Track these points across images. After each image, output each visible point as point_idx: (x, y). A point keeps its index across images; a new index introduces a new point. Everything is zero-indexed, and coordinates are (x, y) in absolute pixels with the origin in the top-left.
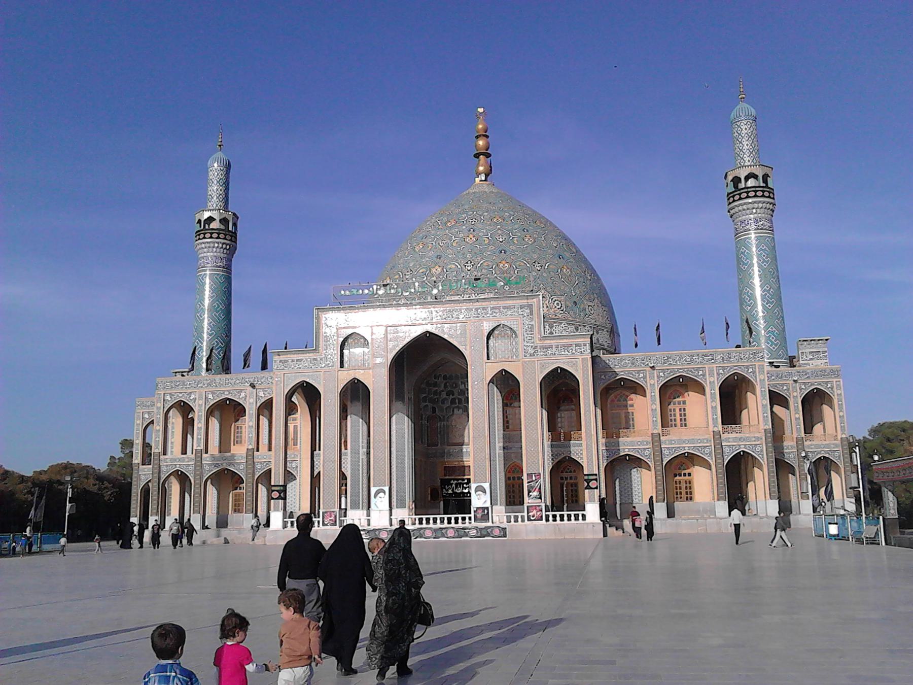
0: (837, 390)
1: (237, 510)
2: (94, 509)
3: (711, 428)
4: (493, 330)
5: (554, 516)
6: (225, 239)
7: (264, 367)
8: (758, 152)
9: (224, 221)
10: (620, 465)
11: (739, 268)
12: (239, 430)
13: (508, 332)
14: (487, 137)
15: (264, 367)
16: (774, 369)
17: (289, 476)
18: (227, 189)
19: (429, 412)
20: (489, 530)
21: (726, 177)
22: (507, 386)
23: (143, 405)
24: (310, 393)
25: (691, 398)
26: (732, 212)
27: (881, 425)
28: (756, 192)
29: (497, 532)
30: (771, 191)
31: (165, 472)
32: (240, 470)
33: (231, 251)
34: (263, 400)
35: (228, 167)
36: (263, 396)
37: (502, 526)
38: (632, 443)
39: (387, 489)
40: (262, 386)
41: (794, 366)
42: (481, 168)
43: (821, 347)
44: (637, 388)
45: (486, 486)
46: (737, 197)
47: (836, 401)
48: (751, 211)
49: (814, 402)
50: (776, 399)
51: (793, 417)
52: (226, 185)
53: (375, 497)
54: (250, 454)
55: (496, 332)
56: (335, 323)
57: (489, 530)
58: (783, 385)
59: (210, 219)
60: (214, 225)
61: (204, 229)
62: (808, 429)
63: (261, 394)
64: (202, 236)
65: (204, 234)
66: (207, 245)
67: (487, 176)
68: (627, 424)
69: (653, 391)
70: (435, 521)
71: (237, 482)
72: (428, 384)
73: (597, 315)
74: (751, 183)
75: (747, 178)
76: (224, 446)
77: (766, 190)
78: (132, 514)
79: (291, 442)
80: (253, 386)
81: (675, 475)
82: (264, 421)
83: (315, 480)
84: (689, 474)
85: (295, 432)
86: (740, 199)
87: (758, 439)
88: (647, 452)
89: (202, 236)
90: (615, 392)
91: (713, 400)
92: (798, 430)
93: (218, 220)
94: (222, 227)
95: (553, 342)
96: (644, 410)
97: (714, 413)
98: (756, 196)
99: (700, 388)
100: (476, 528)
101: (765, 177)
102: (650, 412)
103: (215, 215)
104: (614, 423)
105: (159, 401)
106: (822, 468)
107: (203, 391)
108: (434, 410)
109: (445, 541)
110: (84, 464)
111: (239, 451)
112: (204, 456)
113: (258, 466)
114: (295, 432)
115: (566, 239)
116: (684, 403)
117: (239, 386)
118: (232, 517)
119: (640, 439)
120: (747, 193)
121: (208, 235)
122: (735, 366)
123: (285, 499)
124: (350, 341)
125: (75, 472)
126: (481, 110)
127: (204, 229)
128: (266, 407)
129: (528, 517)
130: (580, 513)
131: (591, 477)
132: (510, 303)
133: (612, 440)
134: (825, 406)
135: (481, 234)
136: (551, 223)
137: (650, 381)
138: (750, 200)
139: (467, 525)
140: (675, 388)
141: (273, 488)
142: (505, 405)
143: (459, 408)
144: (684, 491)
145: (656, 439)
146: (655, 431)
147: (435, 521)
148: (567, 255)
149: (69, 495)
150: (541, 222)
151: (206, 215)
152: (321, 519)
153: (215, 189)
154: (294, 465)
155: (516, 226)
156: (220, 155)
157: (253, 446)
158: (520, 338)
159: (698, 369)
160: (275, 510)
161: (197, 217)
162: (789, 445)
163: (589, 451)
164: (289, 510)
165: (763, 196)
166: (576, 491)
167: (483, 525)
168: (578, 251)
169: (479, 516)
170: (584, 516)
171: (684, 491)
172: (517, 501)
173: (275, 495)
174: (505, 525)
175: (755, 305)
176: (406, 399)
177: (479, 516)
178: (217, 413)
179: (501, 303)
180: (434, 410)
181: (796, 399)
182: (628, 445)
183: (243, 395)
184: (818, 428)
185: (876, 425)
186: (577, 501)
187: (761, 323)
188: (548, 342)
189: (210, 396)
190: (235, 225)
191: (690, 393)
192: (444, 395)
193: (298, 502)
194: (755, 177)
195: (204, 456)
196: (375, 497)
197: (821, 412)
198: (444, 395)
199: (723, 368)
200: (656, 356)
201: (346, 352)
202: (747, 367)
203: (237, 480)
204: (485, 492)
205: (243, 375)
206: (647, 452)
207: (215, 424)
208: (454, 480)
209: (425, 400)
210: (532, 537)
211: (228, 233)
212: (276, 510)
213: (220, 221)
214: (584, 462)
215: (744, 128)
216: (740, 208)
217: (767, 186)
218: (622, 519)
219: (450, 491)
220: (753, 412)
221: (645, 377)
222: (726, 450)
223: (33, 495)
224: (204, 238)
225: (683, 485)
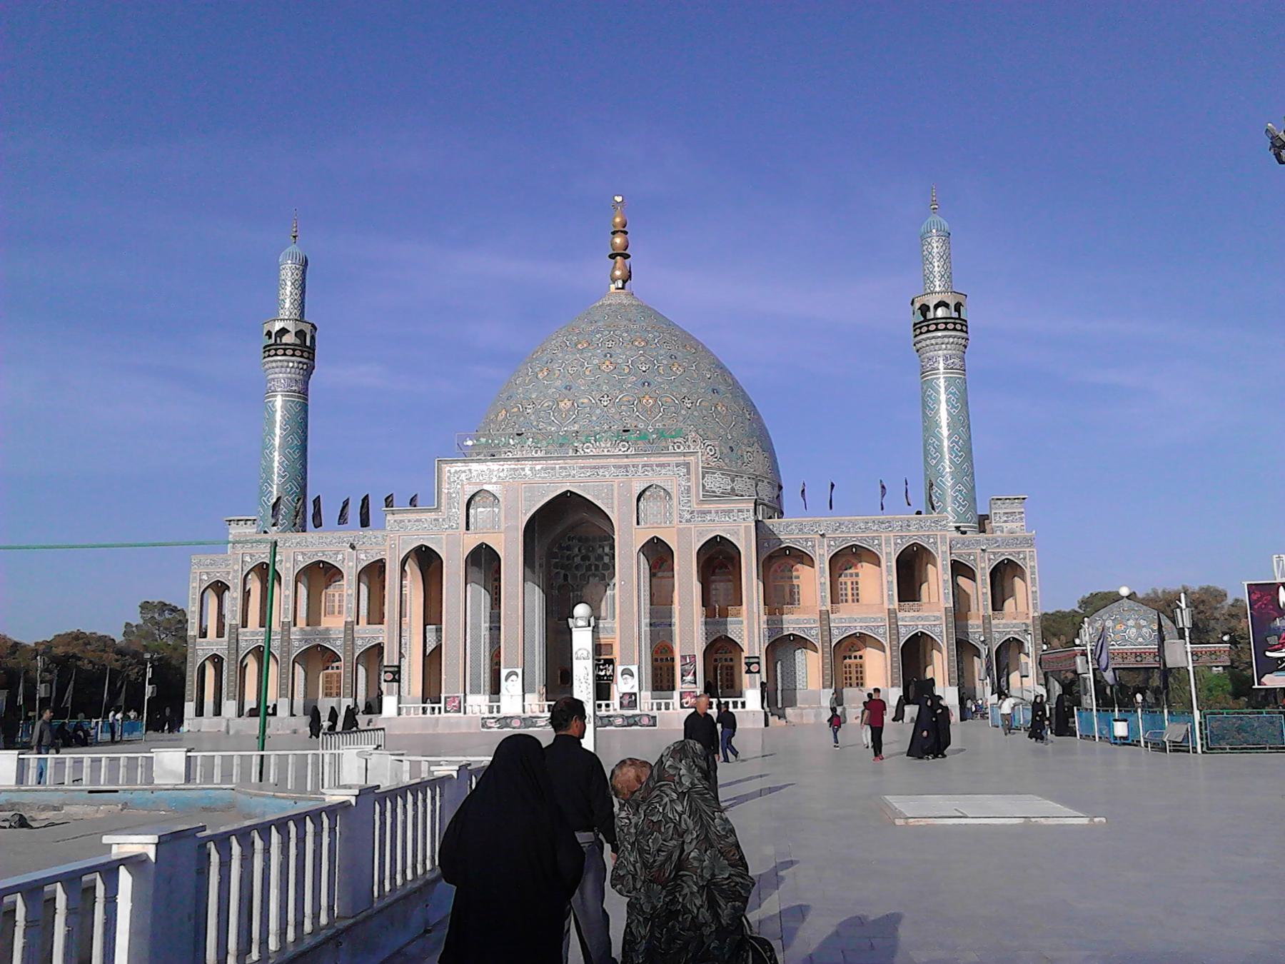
0: (1030, 561)
2: (110, 688)
3: (886, 606)
4: (644, 491)
5: (433, 709)
7: (365, 523)
8: (948, 276)
9: (300, 334)
10: (783, 646)
11: (924, 413)
13: (662, 493)
14: (626, 233)
15: (365, 523)
16: (959, 535)
18: (303, 292)
19: (561, 581)
21: (912, 303)
22: (658, 555)
23: (199, 564)
24: (427, 560)
25: (865, 569)
26: (919, 346)
27: (1094, 596)
28: (946, 324)
29: (645, 721)
30: (964, 323)
31: (245, 646)
32: (337, 647)
33: (309, 371)
37: (651, 714)
38: (797, 622)
39: (519, 671)
40: (363, 547)
41: (984, 532)
42: (618, 273)
43: (1017, 508)
44: (804, 558)
45: (634, 669)
46: (925, 329)
47: (1028, 572)
48: (941, 349)
49: (1004, 574)
50: (960, 569)
51: (979, 591)
52: (302, 287)
53: (506, 680)
55: (647, 493)
56: (462, 476)
58: (969, 555)
59: (283, 331)
60: (288, 339)
61: (274, 345)
62: (997, 605)
63: (363, 556)
64: (272, 352)
67: (624, 282)
68: (791, 598)
69: (822, 564)
72: (561, 548)
73: (758, 463)
74: (940, 312)
75: (936, 307)
77: (959, 324)
78: (187, 697)
80: (353, 547)
81: (845, 658)
83: (432, 660)
86: (928, 331)
87: (937, 618)
88: (814, 632)
89: (272, 352)
90: (780, 560)
91: (889, 573)
92: (985, 607)
94: (298, 342)
95: (713, 507)
96: (811, 583)
97: (890, 589)
98: (946, 329)
99: (877, 561)
101: (958, 307)
102: (818, 586)
103: (290, 326)
104: (778, 598)
105: (236, 562)
106: (1011, 647)
107: (296, 551)
108: (566, 577)
110: (100, 633)
111: (333, 624)
112: (293, 629)
113: (359, 642)
115: (722, 368)
116: (857, 575)
117: (343, 548)
119: (806, 617)
120: (937, 324)
122: (915, 535)
123: (399, 681)
124: (477, 499)
125: (89, 644)
126: (619, 199)
127: (274, 345)
132: (663, 460)
133: (774, 617)
134: (1016, 579)
135: (620, 361)
136: (703, 347)
138: (939, 334)
139: (612, 712)
140: (847, 558)
142: (652, 575)
143: (595, 576)
144: (854, 676)
145: (825, 617)
146: (824, 608)
148: (722, 388)
149: (149, 675)
150: (692, 347)
151: (278, 326)
152: (442, 705)
153: (288, 292)
155: (662, 352)
156: (293, 248)
157: (352, 618)
158: (675, 500)
159: (873, 538)
161: (267, 328)
162: (975, 624)
163: (749, 629)
165: (954, 329)
166: (732, 674)
167: (630, 712)
168: (735, 383)
169: (626, 702)
170: (743, 704)
171: (854, 676)
172: (665, 684)
174: (655, 712)
175: (942, 459)
176: (537, 566)
177: (626, 702)
178: (304, 579)
179: (654, 460)
180: (566, 577)
181: (983, 570)
182: (792, 623)
183: (340, 557)
184: (1009, 603)
185: (1087, 595)
186: (732, 687)
187: (949, 481)
188: (706, 507)
189: (300, 558)
190: (313, 338)
192: (578, 560)
194: (946, 305)
195: (293, 629)
196: (506, 680)
197: (1013, 584)
198: (578, 560)
199: (902, 538)
200: (827, 522)
201: (472, 511)
202: (928, 537)
204: (632, 675)
205: (337, 534)
206: (814, 632)
207: (303, 591)
209: (556, 566)
214: (745, 645)
215: (936, 246)
216: (928, 342)
217: (959, 318)
218: (783, 708)
220: (934, 587)
221: (813, 546)
222: (902, 630)
223: (51, 672)
225: (853, 669)
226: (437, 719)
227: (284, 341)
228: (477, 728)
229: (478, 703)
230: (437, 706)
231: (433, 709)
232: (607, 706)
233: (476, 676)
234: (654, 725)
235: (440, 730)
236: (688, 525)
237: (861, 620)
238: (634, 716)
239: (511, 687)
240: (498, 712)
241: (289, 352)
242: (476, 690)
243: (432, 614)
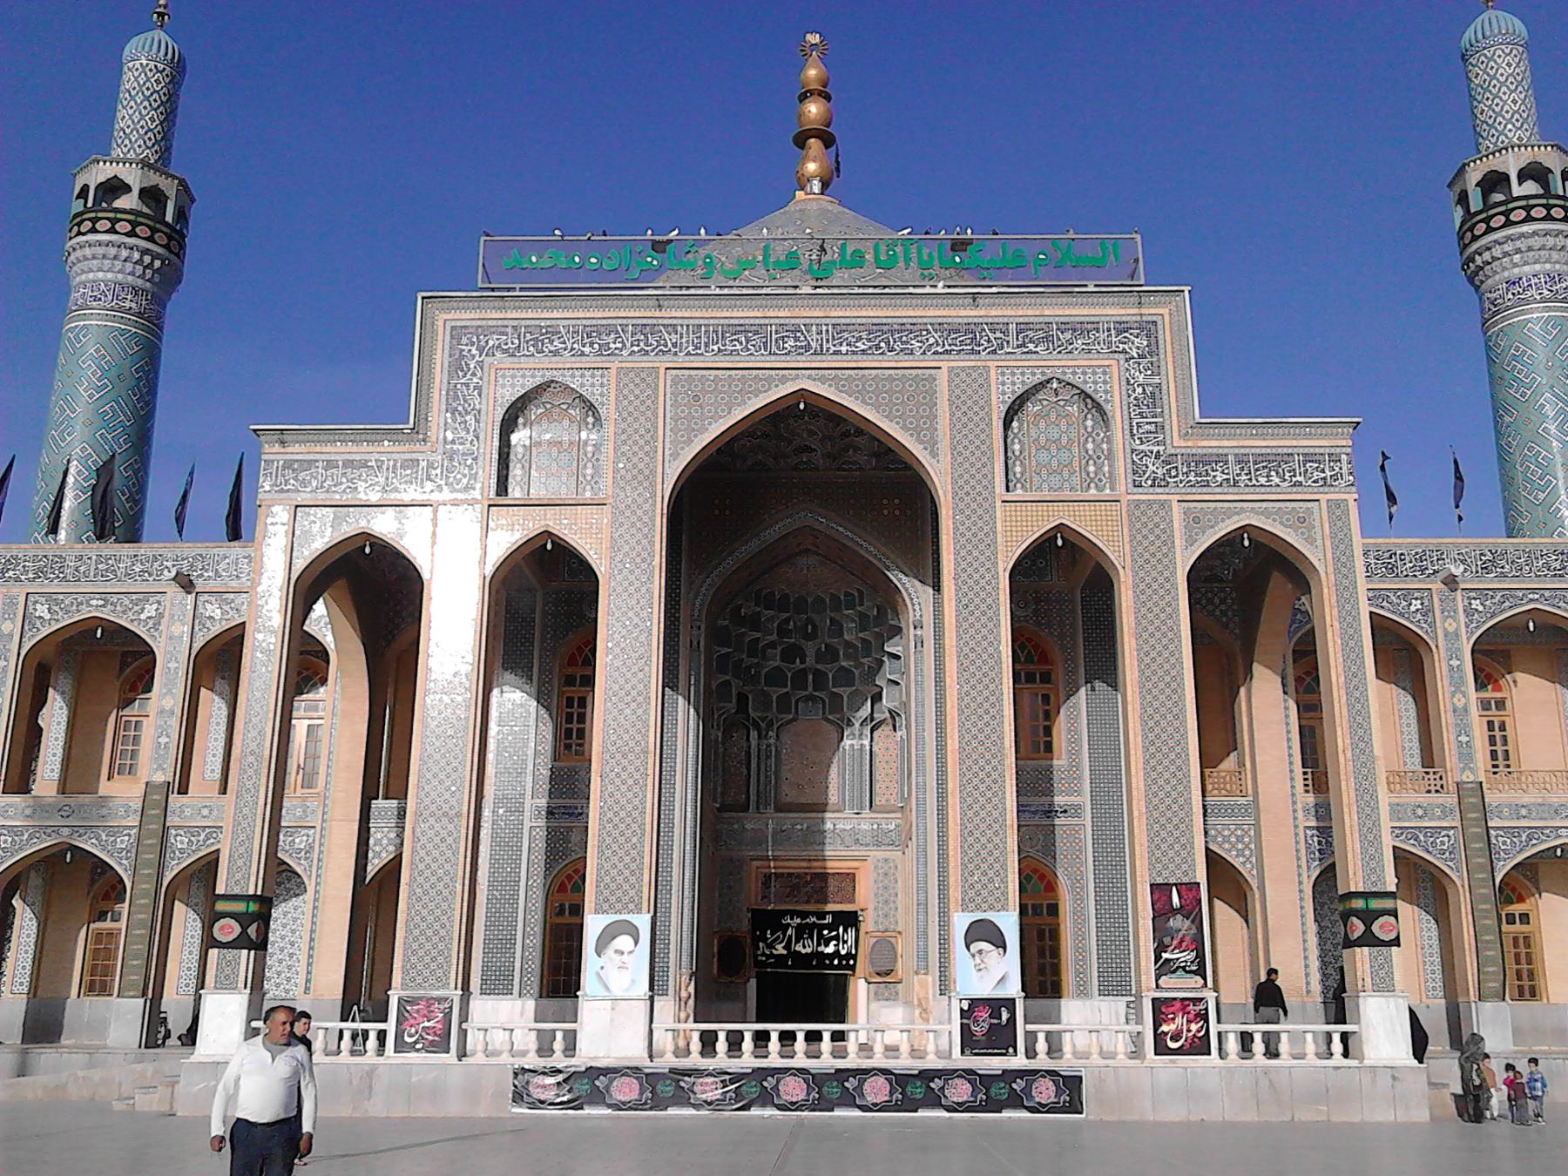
1: (97, 985)
5: (1246, 1039)
6: (150, 239)
9: (152, 195)
12: (129, 735)
14: (828, 98)
17: (282, 878)
20: (1018, 1085)
29: (1045, 1091)
34: (216, 629)
35: (177, 70)
36: (218, 619)
39: (643, 921)
42: (812, 167)
54: (158, 800)
57: (1018, 1085)
59: (114, 188)
60: (127, 202)
65: (94, 221)
66: (100, 251)
70: (735, 1042)
71: (106, 897)
76: (79, 773)
79: (292, 777)
82: (213, 706)
83: (375, 896)
84: (1525, 918)
85: (311, 756)
86: (1509, 223)
93: (136, 192)
100: (968, 1074)
103: (133, 176)
108: (742, 699)
109: (862, 1124)
111: (123, 794)
114: (311, 756)
118: (79, 1008)
121: (103, 225)
123: (261, 945)
126: (813, 39)
128: (221, 660)
129: (1159, 1038)
130: (827, 1028)
131: (1375, 904)
137: (1444, 625)
141: (221, 906)
147: (735, 1042)
152: (391, 1026)
154: (300, 842)
158: (1118, 424)
160: (221, 986)
164: (274, 992)
169: (979, 1029)
173: (227, 930)
178: (64, 680)
180: (742, 699)
183: (150, 610)
190: (181, 214)
191: (1519, 676)
193: (302, 968)
203: (103, 887)
204: (1001, 944)
208: (793, 914)
210: (1175, 1113)
211: (166, 228)
212: (225, 985)
213: (142, 191)
219: (780, 949)
221: (1427, 612)
224: (93, 230)
226: (372, 1071)
227: (118, 204)
228: (497, 1106)
229: (505, 1022)
230: (373, 1027)
232: (838, 1036)
233: (501, 944)
234: (1074, 1106)
235: (376, 1108)
236: (1160, 495)
238: (1009, 1075)
239: (615, 972)
240: (570, 1048)
241: (123, 227)
242: (498, 985)
243: (385, 769)
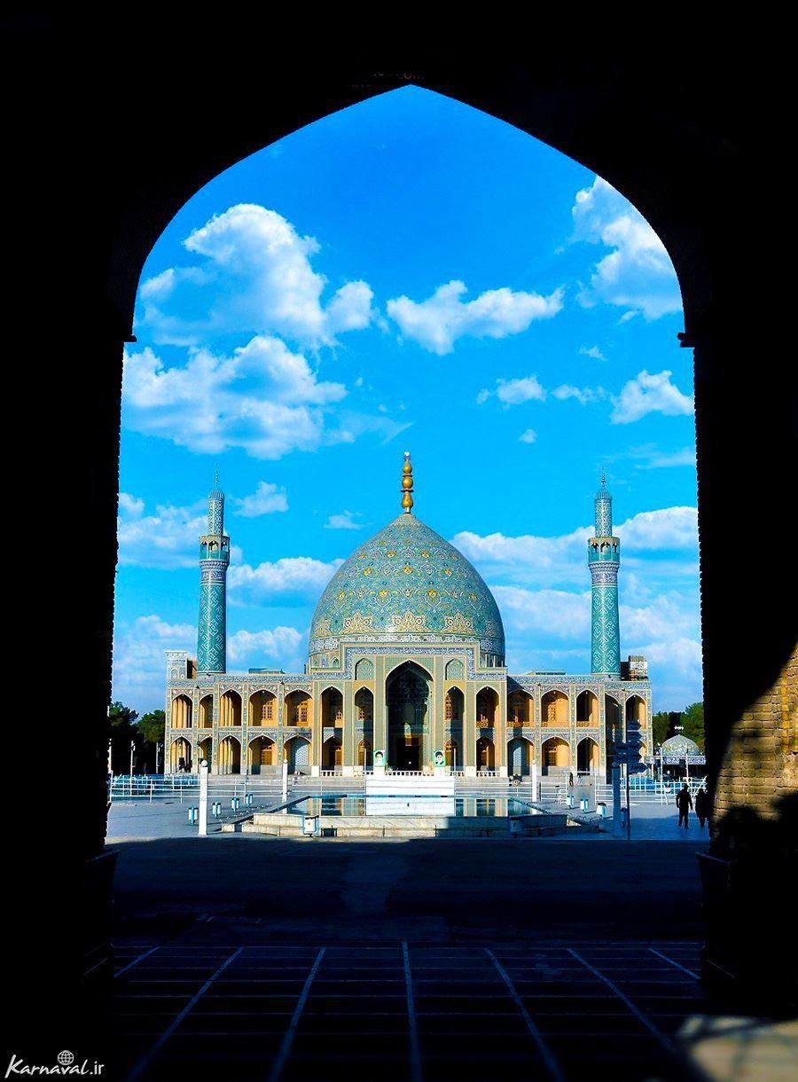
5: (329, 773)
25: (560, 702)
67: (410, 508)
90: (518, 697)
91: (573, 706)
122: (587, 687)
231: (329, 773)
237: (558, 730)
